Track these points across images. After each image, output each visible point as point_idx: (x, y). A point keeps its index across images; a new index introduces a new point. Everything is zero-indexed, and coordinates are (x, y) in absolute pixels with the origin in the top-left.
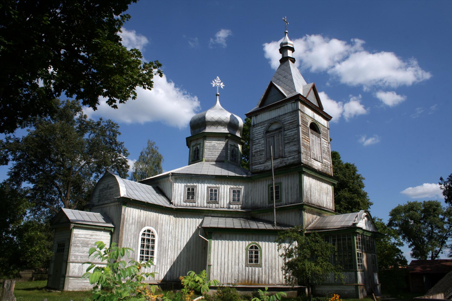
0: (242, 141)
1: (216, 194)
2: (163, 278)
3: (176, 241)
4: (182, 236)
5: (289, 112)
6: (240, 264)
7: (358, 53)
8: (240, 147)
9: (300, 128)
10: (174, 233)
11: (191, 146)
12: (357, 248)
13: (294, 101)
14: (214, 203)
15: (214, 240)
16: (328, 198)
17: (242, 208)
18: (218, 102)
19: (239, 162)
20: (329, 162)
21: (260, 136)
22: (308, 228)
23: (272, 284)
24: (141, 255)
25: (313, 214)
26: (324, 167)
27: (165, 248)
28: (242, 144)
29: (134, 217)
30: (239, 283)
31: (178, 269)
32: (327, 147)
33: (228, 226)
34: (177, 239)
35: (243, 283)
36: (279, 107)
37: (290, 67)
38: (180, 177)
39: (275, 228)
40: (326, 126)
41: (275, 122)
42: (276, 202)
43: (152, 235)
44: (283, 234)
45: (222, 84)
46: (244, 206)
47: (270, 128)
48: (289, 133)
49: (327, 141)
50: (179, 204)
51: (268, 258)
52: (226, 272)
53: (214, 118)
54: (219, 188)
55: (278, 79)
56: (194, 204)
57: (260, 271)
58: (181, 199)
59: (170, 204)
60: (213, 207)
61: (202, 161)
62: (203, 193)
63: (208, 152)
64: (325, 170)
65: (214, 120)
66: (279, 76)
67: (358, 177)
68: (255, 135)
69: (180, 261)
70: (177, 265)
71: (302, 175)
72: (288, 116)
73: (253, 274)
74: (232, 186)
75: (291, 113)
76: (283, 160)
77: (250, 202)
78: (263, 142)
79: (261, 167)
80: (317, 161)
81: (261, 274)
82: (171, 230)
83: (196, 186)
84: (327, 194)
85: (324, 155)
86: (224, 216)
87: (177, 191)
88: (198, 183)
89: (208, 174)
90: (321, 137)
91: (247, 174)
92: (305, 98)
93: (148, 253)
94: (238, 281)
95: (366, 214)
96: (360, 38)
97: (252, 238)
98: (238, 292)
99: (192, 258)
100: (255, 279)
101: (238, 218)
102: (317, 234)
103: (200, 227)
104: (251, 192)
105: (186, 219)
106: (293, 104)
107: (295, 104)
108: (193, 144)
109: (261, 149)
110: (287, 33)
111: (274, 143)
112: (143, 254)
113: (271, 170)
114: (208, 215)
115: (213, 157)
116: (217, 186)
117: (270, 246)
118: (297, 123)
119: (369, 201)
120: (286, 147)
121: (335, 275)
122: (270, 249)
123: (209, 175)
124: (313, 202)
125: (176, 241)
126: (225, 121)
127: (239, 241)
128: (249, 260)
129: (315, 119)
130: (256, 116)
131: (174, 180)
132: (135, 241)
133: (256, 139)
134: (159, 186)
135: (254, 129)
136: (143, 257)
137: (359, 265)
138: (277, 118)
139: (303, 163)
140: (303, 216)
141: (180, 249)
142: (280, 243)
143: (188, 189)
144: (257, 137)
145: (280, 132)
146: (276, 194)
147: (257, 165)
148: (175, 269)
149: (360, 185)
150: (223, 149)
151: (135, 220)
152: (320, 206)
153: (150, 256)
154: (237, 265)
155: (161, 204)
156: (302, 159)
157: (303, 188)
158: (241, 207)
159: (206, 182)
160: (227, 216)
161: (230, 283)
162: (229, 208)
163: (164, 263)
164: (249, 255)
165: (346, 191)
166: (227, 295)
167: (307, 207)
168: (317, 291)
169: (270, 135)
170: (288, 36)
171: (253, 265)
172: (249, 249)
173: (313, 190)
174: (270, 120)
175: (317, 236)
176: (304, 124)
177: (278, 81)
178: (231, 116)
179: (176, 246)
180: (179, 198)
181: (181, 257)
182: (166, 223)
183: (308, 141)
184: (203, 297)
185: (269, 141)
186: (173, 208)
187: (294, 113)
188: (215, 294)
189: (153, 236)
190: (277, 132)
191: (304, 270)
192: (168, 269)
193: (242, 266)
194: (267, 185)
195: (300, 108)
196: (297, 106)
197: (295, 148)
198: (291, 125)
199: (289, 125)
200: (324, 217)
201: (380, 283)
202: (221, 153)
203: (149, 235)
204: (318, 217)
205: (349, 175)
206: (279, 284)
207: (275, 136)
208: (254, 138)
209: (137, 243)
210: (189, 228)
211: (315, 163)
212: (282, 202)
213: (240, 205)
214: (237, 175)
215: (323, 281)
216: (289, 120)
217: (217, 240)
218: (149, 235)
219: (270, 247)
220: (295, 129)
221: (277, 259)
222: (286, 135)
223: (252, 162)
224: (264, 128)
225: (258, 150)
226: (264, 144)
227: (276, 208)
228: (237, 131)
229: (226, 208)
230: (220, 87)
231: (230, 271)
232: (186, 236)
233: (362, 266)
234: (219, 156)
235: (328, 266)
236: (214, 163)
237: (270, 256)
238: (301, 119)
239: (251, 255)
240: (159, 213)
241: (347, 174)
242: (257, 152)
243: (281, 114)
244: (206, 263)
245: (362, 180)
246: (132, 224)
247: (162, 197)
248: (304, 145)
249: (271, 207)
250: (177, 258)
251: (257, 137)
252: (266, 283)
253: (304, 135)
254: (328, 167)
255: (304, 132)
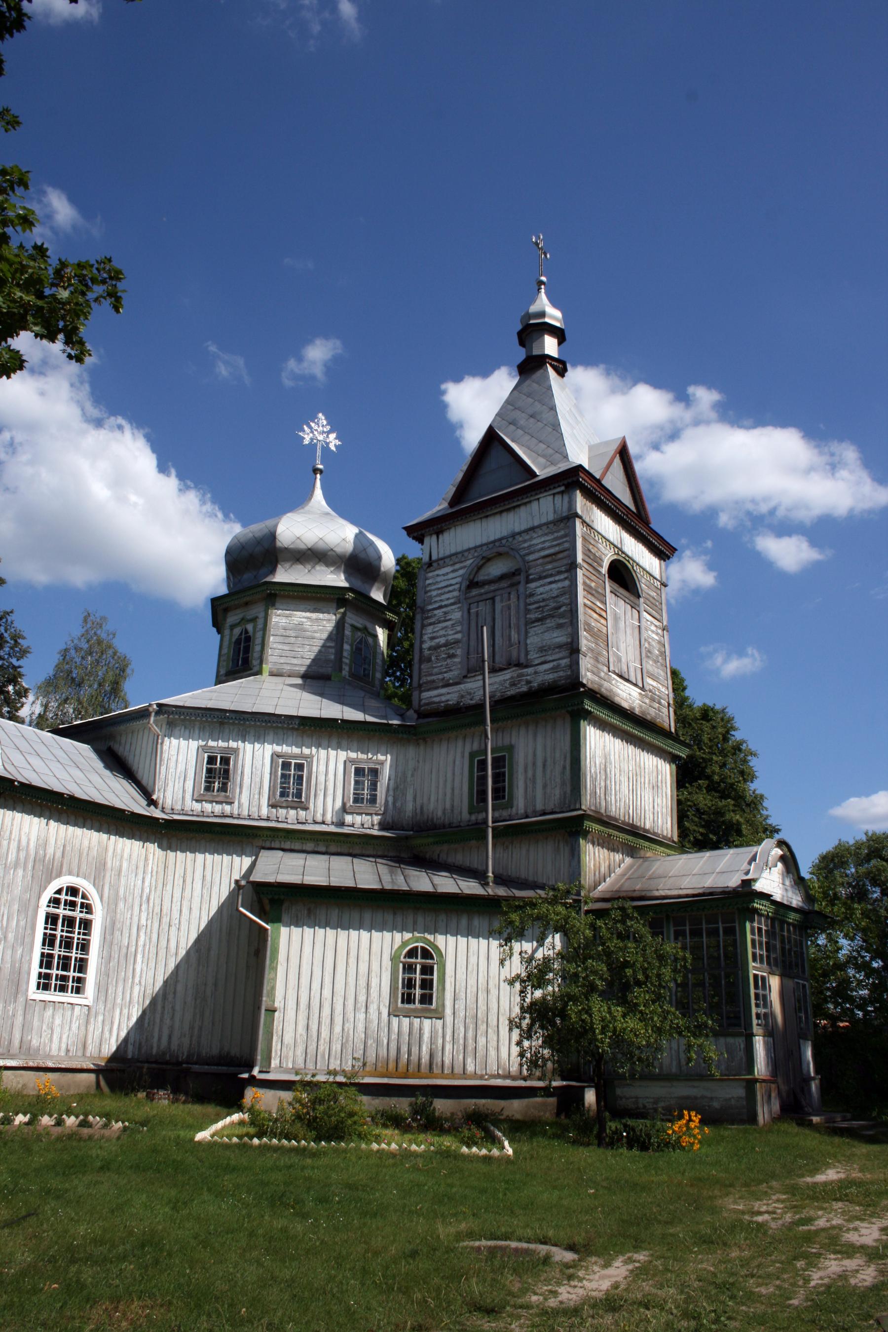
0: (390, 616)
1: (300, 778)
2: (114, 1048)
3: (165, 926)
4: (185, 911)
5: (544, 524)
6: (373, 1008)
7: (701, 430)
8: (382, 634)
9: (580, 573)
10: (158, 901)
11: (227, 625)
12: (754, 960)
13: (563, 488)
14: (292, 808)
15: (288, 925)
16: (660, 801)
17: (383, 826)
18: (318, 493)
19: (377, 683)
20: (663, 689)
21: (447, 596)
22: (596, 894)
23: (475, 1076)
24: (44, 971)
25: (613, 849)
26: (647, 701)
27: (124, 950)
28: (389, 626)
29: (24, 843)
30: (368, 1069)
31: (168, 1021)
32: (659, 642)
33: (335, 882)
34: (166, 920)
35: (379, 1069)
36: (514, 508)
37: (550, 388)
38: (185, 720)
39: (491, 892)
40: (658, 577)
41: (500, 554)
42: (493, 810)
43: (82, 904)
44: (519, 907)
45: (332, 436)
46: (389, 819)
47: (482, 572)
48: (541, 590)
49: (657, 623)
50: (178, 807)
51: (463, 990)
52: (325, 1033)
53: (303, 538)
54: (309, 757)
55: (513, 423)
56: (227, 808)
57: (437, 1032)
58: (184, 791)
59: (149, 805)
60: (290, 818)
61: (259, 672)
62: (259, 773)
63: (280, 647)
64: (652, 714)
65: (303, 547)
66: (517, 414)
67: (737, 748)
68: (434, 593)
69: (175, 993)
70: (163, 1007)
71: (583, 723)
72: (543, 535)
73: (413, 1041)
74: (353, 755)
75: (551, 526)
76: (522, 675)
77: (410, 807)
78: (457, 615)
79: (448, 697)
80: (628, 680)
81: (440, 1041)
82: (147, 890)
83: (236, 751)
84: (655, 787)
85: (649, 665)
86: (323, 849)
87: (172, 764)
88: (244, 742)
89: (277, 712)
90: (642, 609)
91: (402, 716)
92: (598, 482)
93: (65, 964)
94: (364, 1064)
95: (780, 852)
96: (710, 385)
97: (415, 923)
98: (365, 1099)
99: (216, 985)
100: (420, 1059)
101: (368, 856)
102: (630, 911)
103: (243, 883)
104: (413, 775)
105: (200, 857)
106: (558, 498)
107: (566, 498)
108: (232, 619)
109: (450, 638)
110: (542, 283)
111: (494, 619)
112: (49, 966)
113: (481, 706)
114: (273, 846)
115: (295, 661)
116: (306, 751)
117: (471, 950)
118: (569, 556)
119: (769, 822)
120: (532, 632)
121: (689, 1047)
122: (473, 960)
123: (280, 716)
124: (613, 811)
125: (165, 926)
126: (339, 550)
127: (370, 931)
128: (403, 994)
129: (626, 549)
130: (438, 533)
131: (164, 726)
132: (22, 923)
133: (437, 605)
134: (116, 747)
135: (430, 575)
136: (48, 976)
137: (758, 1016)
138: (504, 541)
139: (584, 685)
140: (582, 856)
141: (176, 954)
142: (508, 940)
143: (209, 757)
144: (438, 599)
145: (512, 585)
146: (495, 782)
147: (437, 688)
148: (158, 1020)
149: (742, 773)
150: (330, 638)
151: (27, 851)
152: (633, 826)
153: (71, 974)
154: (363, 1010)
155: (119, 804)
156: (583, 671)
157: (582, 763)
158: (380, 824)
159: (271, 737)
160: (333, 849)
161: (338, 1068)
162: (342, 824)
163: (119, 1001)
164: (403, 979)
165: (700, 787)
166: (325, 1113)
167: (595, 827)
168: (621, 1098)
169: (481, 594)
170: (546, 293)
171: (415, 1010)
172: (402, 959)
173: (613, 771)
174: (482, 546)
175: (631, 919)
176: (590, 561)
177: (512, 427)
178: (357, 536)
179: (163, 943)
180: (179, 786)
181: (177, 982)
182: (134, 867)
183: (601, 616)
184: (246, 1116)
185: (477, 614)
186: (158, 819)
187: (562, 525)
188: (286, 1105)
189: (88, 908)
190: (504, 584)
191: (586, 1030)
192: (134, 1020)
193: (380, 1013)
194: (467, 755)
195: (579, 511)
196: (572, 503)
197: (559, 637)
198: (550, 562)
199: (542, 564)
200: (645, 859)
201: (817, 1071)
202: (320, 651)
203: (73, 904)
204: (628, 860)
205: (710, 740)
206: (498, 1076)
207: (498, 599)
208: (431, 604)
209: (29, 931)
210: (208, 885)
211: (622, 687)
212: (514, 809)
213: (377, 814)
214: (370, 719)
215: (648, 1066)
216: (543, 549)
217: (297, 926)
218: (73, 904)
219: (470, 954)
220: (562, 577)
221: (494, 992)
222: (532, 595)
223: (420, 679)
224: (461, 572)
225: (442, 641)
226: (461, 623)
227: (494, 829)
228: (376, 585)
229: (333, 823)
230: (326, 449)
231: (338, 1029)
232: (196, 912)
233: (767, 1018)
234: (314, 660)
235: (665, 1018)
236: (299, 681)
237: (472, 982)
238: (584, 546)
239: (410, 980)
240: (109, 832)
241: (705, 738)
242: (438, 647)
243: (517, 530)
244: (260, 1001)
245: (749, 758)
246: (16, 865)
247: (125, 783)
248: (589, 629)
249: (477, 824)
250: (166, 983)
251: (438, 599)
252: (456, 1071)
253: (589, 596)
254: (660, 703)
255: (590, 587)
